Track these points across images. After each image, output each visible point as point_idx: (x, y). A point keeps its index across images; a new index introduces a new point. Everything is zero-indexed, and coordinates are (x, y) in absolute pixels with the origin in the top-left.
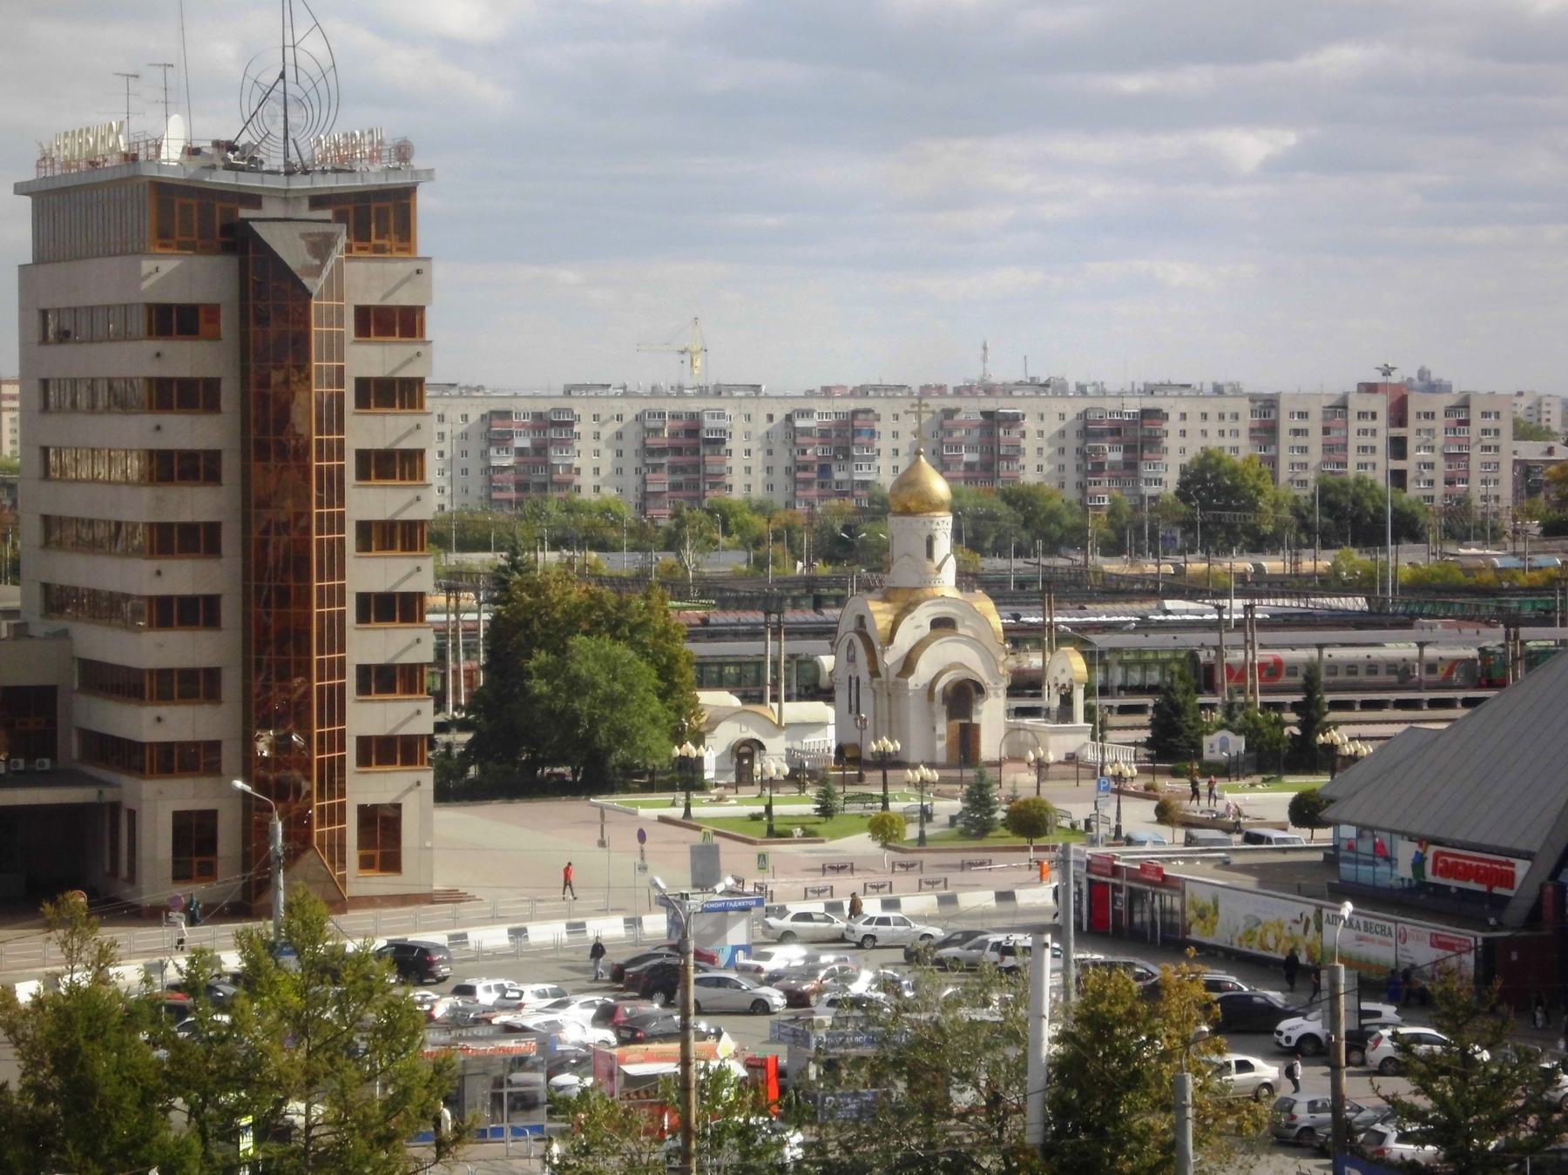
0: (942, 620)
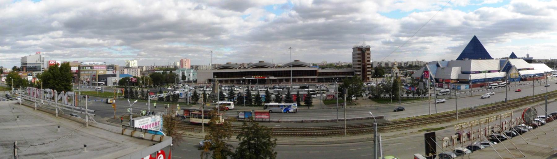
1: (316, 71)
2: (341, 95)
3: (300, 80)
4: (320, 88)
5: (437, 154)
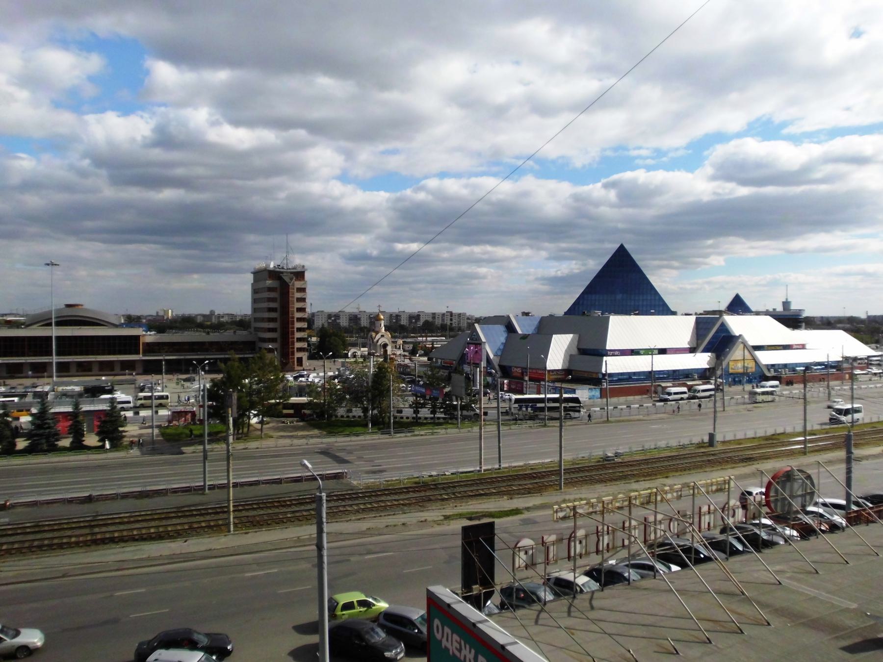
0: (383, 337)
1: (137, 338)
2: (218, 413)
3: (84, 369)
4: (151, 389)
5: (498, 588)
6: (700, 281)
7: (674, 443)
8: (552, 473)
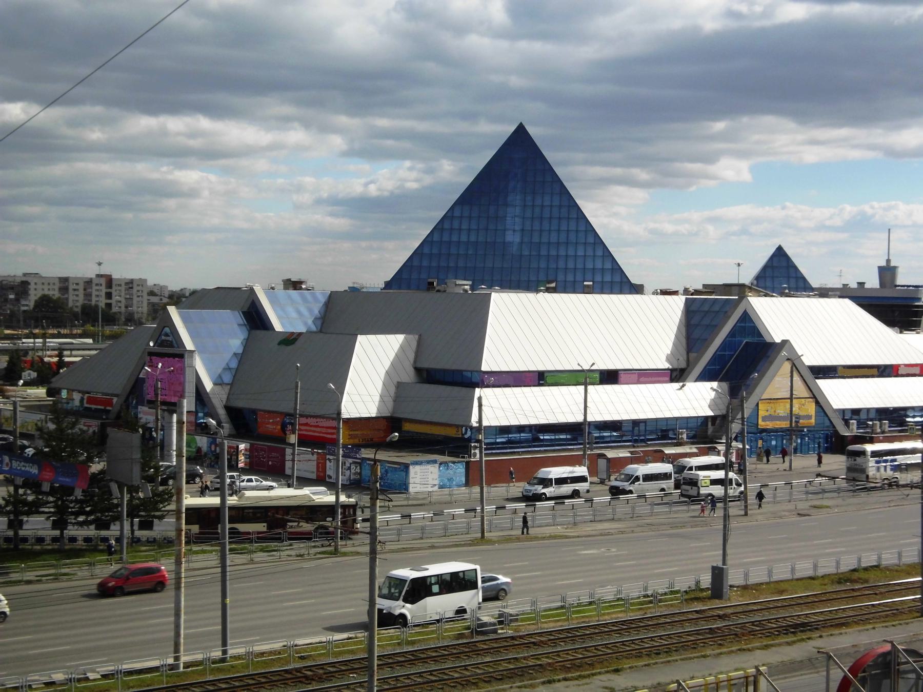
6: (696, 216)
7: (633, 591)
8: (349, 666)
